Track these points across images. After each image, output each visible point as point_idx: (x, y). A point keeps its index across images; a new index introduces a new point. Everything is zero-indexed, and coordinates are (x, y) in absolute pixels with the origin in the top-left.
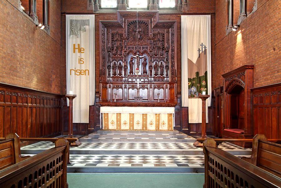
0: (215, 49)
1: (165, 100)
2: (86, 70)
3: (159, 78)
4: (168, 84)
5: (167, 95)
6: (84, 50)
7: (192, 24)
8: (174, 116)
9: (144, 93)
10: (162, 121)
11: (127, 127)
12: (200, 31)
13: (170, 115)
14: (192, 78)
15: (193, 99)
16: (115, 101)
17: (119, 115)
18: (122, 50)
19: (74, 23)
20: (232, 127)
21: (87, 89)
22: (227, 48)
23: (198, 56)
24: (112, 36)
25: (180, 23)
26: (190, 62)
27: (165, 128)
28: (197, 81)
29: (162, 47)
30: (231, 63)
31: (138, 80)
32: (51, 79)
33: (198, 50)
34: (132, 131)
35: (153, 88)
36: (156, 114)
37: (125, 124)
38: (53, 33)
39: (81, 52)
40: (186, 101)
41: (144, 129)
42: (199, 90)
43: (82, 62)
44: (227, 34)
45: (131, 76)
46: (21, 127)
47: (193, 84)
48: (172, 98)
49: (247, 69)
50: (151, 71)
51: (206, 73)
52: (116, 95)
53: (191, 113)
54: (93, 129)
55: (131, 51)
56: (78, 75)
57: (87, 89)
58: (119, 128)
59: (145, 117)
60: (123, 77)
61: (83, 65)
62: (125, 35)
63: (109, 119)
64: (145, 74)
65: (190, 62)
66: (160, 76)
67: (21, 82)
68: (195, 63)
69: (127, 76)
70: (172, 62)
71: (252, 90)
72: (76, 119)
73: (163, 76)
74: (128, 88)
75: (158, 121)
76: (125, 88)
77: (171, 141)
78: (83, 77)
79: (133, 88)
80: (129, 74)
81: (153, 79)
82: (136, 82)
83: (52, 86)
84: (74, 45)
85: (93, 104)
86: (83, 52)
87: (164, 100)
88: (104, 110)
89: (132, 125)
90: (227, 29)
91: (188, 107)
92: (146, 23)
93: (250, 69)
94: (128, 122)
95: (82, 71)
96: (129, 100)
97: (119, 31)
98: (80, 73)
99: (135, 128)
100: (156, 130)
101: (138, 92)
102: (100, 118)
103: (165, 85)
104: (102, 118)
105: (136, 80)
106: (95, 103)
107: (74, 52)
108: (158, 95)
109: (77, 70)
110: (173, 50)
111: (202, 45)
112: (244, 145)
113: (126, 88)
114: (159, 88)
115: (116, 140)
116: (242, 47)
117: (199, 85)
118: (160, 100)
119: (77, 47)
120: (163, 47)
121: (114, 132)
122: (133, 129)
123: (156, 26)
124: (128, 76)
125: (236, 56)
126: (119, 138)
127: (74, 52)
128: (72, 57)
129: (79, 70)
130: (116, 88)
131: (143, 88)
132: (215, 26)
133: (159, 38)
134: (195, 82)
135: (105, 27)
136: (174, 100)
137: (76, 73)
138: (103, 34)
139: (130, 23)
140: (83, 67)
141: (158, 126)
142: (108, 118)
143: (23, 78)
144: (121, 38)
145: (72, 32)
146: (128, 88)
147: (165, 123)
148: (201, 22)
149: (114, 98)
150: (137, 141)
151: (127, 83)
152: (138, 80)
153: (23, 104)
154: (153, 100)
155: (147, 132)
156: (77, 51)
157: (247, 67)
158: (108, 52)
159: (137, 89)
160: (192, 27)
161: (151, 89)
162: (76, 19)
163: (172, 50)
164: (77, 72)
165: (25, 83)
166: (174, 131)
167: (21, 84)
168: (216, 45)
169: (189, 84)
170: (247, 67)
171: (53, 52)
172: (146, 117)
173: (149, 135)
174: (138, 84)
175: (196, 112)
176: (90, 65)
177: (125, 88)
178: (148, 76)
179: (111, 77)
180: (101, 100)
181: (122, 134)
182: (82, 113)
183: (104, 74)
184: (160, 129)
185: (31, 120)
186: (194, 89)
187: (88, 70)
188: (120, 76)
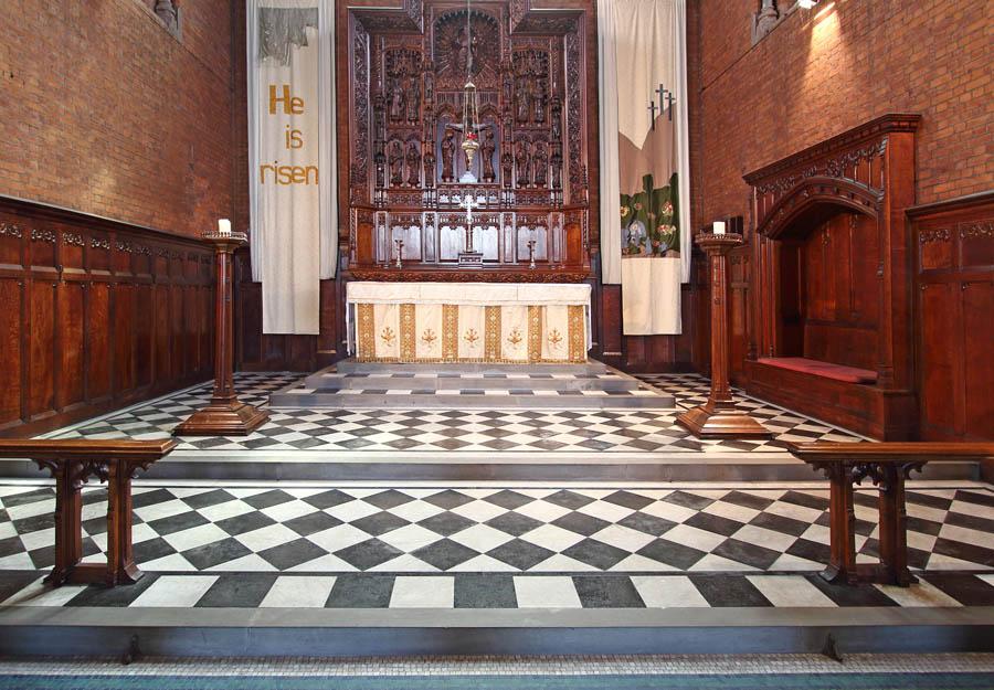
0: (700, 103)
1: (551, 262)
2: (308, 169)
3: (532, 192)
4: (560, 211)
5: (557, 246)
6: (302, 105)
7: (631, 25)
8: (587, 314)
9: (487, 242)
10: (550, 329)
11: (435, 351)
12: (654, 46)
13: (575, 309)
14: (632, 195)
15: (636, 261)
16: (398, 264)
17: (408, 309)
18: (418, 105)
19: (272, 20)
20: (790, 349)
21: (312, 225)
22: (759, 85)
23: (651, 125)
24: (388, 60)
25: (594, 21)
26: (625, 143)
27: (561, 352)
28: (649, 204)
29: (540, 96)
30: (780, 132)
31: (469, 198)
32: (187, 190)
33: (650, 105)
34: (452, 365)
35: (514, 228)
36: (530, 307)
37: (429, 339)
38: (196, 38)
39: (293, 112)
40: (616, 267)
41: (492, 360)
42: (653, 231)
43: (297, 143)
44: (755, 39)
45: (448, 186)
46: (17, 361)
47: (636, 211)
48: (574, 258)
49: (893, 129)
50: (508, 172)
51: (674, 178)
52: (401, 246)
53: (631, 305)
54: (333, 352)
55: (446, 108)
56: (284, 183)
57: (312, 225)
58: (408, 353)
59: (493, 318)
60: (421, 191)
61: (299, 152)
62: (427, 56)
63: (375, 322)
64: (490, 180)
65: (625, 143)
66: (535, 186)
67: (16, 177)
68: (641, 148)
69: (434, 187)
70: (571, 142)
71: (911, 215)
72: (275, 321)
73: (545, 186)
74: (436, 224)
75: (537, 329)
76: (428, 224)
77: (588, 402)
78: (301, 188)
79: (453, 224)
80: (440, 181)
81: (513, 196)
82: (462, 205)
83: (196, 215)
84: (273, 89)
85: (332, 276)
86: (301, 112)
87: (547, 261)
88: (357, 292)
89: (451, 343)
90: (757, 21)
91: (621, 285)
92: (492, 20)
93: (903, 129)
94: (439, 334)
95: (297, 171)
96: (441, 261)
97: (409, 42)
98: (292, 179)
99: (461, 355)
100: (532, 361)
101: (469, 238)
102: (347, 321)
103: (550, 216)
104: (352, 320)
105: (463, 199)
106: (339, 273)
107: (273, 110)
108: (530, 246)
109: (282, 168)
110: (574, 105)
111: (661, 91)
112: (881, 431)
113: (432, 224)
114: (532, 225)
115: (397, 400)
116: (843, 60)
117: (653, 216)
118: (536, 261)
119: (280, 94)
120: (545, 97)
121: (392, 369)
122: (455, 358)
123: (523, 27)
124: (438, 186)
125: (807, 104)
126: (409, 392)
127: (273, 110)
128: (266, 127)
129: (289, 168)
130: (400, 224)
131: (484, 223)
132: (699, 32)
133: (533, 67)
134: (640, 207)
135: (366, 29)
136: (579, 263)
137: (279, 177)
138: (361, 53)
139: (441, 19)
140: (301, 161)
141: (536, 347)
142: (372, 322)
143: (26, 164)
144: (414, 66)
145: (265, 49)
146: (436, 224)
147: (559, 338)
148: (658, 19)
149: (396, 254)
150: (469, 403)
151: (434, 210)
152: (469, 198)
153: (134, 274)
154: (515, 263)
155: (501, 368)
156: (281, 106)
157: (895, 124)
158: (377, 109)
159: (467, 229)
160: (630, 34)
161: (508, 228)
162: (278, 7)
163: (570, 103)
164: (282, 174)
165: (45, 185)
166: (589, 363)
167: (18, 186)
168: (704, 89)
169: (622, 212)
170: (895, 124)
171: (198, 103)
172: (499, 317)
173: (511, 380)
174: (469, 210)
175: (654, 296)
176: (321, 153)
177: (430, 223)
178: (499, 187)
179: (387, 190)
180: (353, 260)
181: (417, 375)
182: (298, 303)
183: (364, 179)
184: (544, 356)
185: (81, 331)
186: (638, 229)
187: (314, 168)
188: (414, 188)
